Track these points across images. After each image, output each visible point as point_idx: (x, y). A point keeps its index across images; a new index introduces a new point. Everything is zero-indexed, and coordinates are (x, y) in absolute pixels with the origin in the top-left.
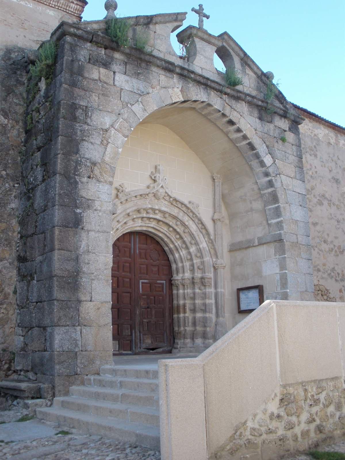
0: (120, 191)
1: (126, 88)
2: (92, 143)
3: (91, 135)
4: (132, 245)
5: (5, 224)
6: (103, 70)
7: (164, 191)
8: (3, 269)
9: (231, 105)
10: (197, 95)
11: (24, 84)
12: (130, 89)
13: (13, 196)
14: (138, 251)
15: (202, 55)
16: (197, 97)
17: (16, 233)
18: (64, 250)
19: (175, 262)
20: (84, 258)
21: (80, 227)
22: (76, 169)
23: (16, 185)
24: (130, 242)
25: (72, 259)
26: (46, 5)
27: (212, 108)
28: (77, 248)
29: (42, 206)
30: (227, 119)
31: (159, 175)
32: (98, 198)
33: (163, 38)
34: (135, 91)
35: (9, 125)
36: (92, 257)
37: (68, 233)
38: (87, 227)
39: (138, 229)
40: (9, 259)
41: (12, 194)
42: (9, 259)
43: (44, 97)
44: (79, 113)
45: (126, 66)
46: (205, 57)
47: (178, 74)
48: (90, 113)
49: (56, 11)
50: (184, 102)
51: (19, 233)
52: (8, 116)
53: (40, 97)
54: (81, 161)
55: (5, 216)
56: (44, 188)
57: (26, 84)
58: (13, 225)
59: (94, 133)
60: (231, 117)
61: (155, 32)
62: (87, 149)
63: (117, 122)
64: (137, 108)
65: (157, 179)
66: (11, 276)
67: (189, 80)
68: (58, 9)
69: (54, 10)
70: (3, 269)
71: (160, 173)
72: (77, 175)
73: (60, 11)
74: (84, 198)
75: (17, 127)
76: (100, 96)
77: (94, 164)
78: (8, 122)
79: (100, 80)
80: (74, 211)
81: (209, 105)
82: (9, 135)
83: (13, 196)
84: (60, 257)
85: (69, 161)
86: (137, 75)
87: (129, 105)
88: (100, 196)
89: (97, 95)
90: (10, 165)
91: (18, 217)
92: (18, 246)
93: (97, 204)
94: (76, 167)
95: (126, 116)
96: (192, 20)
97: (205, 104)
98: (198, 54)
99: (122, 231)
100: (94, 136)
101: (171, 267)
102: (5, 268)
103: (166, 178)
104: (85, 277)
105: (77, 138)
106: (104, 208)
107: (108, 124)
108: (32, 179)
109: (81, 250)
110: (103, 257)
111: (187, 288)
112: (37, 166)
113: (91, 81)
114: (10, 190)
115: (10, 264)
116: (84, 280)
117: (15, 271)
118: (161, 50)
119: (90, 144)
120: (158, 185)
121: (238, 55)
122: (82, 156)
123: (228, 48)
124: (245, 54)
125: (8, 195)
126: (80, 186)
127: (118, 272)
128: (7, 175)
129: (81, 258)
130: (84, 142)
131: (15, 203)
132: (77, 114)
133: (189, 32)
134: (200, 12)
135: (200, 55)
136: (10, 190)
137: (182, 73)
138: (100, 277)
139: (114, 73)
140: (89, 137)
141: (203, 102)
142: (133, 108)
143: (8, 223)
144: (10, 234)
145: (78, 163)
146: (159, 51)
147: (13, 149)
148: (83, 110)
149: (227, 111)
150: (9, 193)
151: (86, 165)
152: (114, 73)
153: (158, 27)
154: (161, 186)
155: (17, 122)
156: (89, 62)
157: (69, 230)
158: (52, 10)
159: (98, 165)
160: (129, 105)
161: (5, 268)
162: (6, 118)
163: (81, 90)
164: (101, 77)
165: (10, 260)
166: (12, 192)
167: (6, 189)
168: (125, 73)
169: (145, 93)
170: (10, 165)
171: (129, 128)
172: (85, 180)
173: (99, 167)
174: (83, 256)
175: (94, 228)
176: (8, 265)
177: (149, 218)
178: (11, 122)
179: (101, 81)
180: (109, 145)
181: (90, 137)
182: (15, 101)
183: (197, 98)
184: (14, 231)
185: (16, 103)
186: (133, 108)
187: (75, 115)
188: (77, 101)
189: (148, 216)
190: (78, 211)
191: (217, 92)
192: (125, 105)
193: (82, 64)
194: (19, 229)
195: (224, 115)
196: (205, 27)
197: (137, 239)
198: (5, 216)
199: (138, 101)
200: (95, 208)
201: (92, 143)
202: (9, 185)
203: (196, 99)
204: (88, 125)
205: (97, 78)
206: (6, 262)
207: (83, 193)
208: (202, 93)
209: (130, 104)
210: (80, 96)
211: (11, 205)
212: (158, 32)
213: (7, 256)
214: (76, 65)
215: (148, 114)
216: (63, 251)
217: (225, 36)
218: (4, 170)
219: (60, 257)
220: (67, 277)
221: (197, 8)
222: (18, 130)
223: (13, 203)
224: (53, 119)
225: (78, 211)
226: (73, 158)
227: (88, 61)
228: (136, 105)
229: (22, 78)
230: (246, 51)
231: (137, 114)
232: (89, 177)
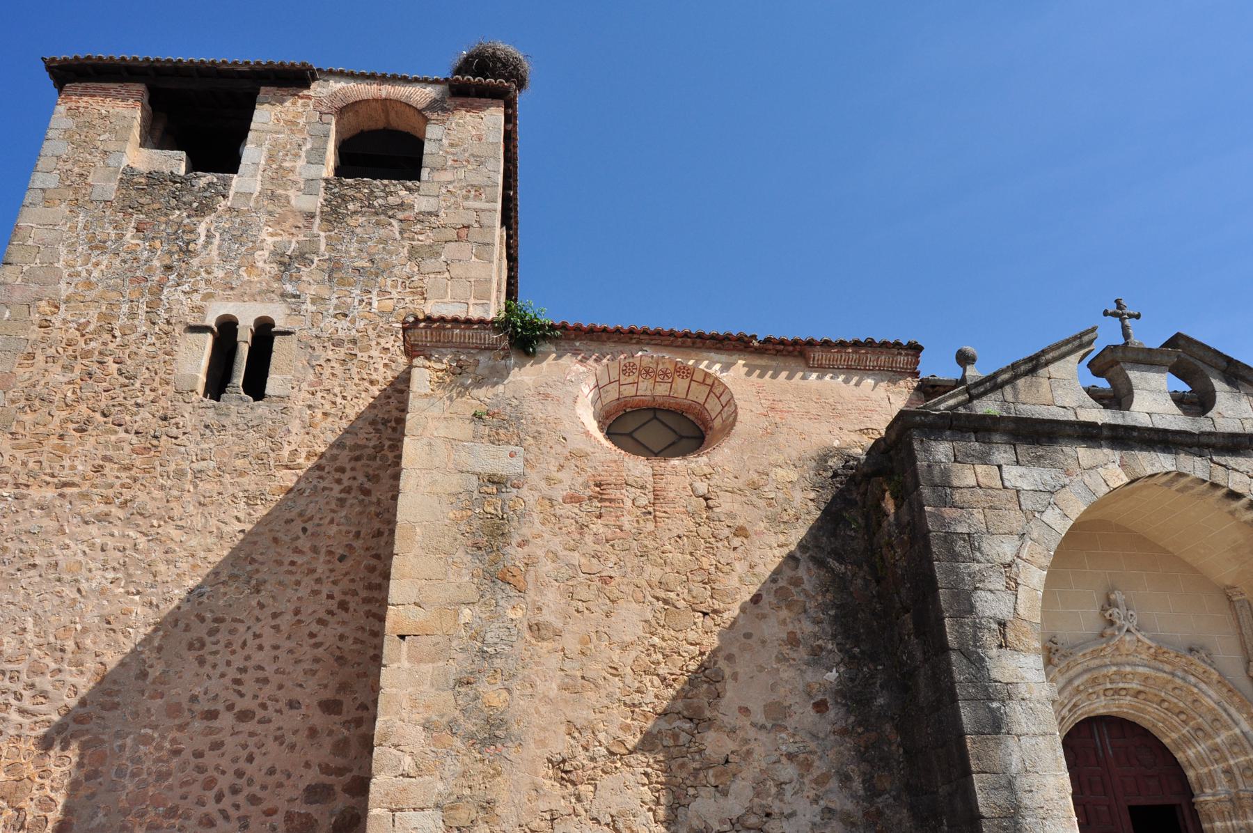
0: (1053, 650)
1: (1025, 488)
2: (991, 591)
3: (987, 577)
4: (1098, 740)
5: (874, 733)
6: (980, 469)
7: (1135, 638)
8: (886, 809)
9: (1224, 463)
10: (1153, 465)
11: (857, 503)
12: (1032, 488)
13: (878, 685)
14: (1111, 752)
15: (1143, 389)
16: (1154, 468)
17: (895, 745)
18: (986, 773)
19: (1191, 765)
20: (1022, 783)
21: (1003, 731)
22: (976, 639)
23: (880, 667)
24: (1092, 737)
25: (1001, 787)
26: (860, 369)
27: (1189, 479)
28: (1006, 767)
29: (933, 702)
30: (1224, 491)
31: (1117, 610)
32: (1023, 679)
33: (1066, 382)
34: (1042, 488)
35: (849, 573)
36: (1033, 779)
37: (987, 744)
38: (1016, 729)
39: (1102, 711)
40: (891, 790)
41: (876, 683)
42: (891, 790)
43: (896, 525)
44: (959, 546)
45: (1015, 451)
46: (1151, 391)
47: (1107, 438)
48: (976, 544)
49: (877, 374)
50: (1132, 482)
51: (899, 746)
52: (843, 559)
53: (889, 525)
54: (981, 624)
55: (873, 720)
56: (930, 672)
57: (860, 504)
58: (887, 733)
59: (991, 573)
60: (1232, 486)
61: (1049, 378)
62: (986, 602)
63: (1024, 548)
64: (1051, 516)
65: (1115, 618)
66: (900, 820)
67: (1130, 443)
68: (879, 369)
69: (874, 374)
70: (886, 809)
71: (1118, 607)
72: (979, 647)
73: (883, 372)
74: (1000, 682)
75: (861, 574)
76: (986, 511)
77: (1002, 624)
78: (846, 568)
79: (979, 485)
80: (988, 707)
81: (1180, 475)
82: (851, 589)
83: (878, 685)
84: (982, 785)
85: (961, 626)
86: (1037, 460)
87: (1037, 515)
88: (1024, 674)
89: (981, 510)
90: (864, 637)
91: (893, 719)
92: (903, 768)
93: (1023, 690)
94: (975, 635)
95: (1035, 535)
96: (1109, 334)
97: (1172, 475)
98: (1135, 391)
99: (1072, 718)
100: (992, 579)
101: (1186, 776)
102: (887, 806)
103: (1132, 613)
104: (1031, 816)
105: (966, 588)
106: (1036, 695)
107: (1009, 554)
108: (904, 658)
109: (1014, 769)
110: (1052, 778)
111: (1230, 816)
112: (909, 636)
113: (965, 490)
114: (872, 676)
115: (895, 800)
116: (1029, 820)
117: (905, 811)
118: (1066, 405)
119: (989, 593)
120: (1120, 629)
121: (1215, 367)
122: (980, 615)
123: (1192, 360)
124: (1229, 360)
125: (870, 685)
126: (989, 664)
127: (1082, 794)
128: (862, 652)
129: (1018, 783)
130: (979, 592)
131: (883, 697)
132: (957, 549)
133: (1109, 357)
134: (1118, 312)
135: (1139, 392)
136: (872, 676)
137: (1114, 434)
138: (1055, 812)
139: (1000, 467)
140: (984, 581)
141: (1167, 473)
142: (1044, 518)
143: (879, 731)
144: (886, 749)
145: (977, 627)
146: (1065, 407)
147: (863, 610)
148: (964, 540)
149: (1219, 476)
150: (871, 682)
151: (989, 629)
152: (1000, 467)
153: (1052, 368)
154: (1125, 630)
155: (860, 567)
156: (956, 461)
157: (988, 739)
158: (872, 375)
159: (1009, 624)
160: (1037, 515)
161: (887, 806)
162: (841, 564)
163: (954, 509)
164: (981, 480)
165: (894, 793)
166: (875, 680)
167: (865, 676)
168: (1018, 463)
169: (1057, 488)
170: (864, 637)
171: (1046, 552)
172: (994, 652)
173: (1013, 627)
174: (1019, 779)
175: (1025, 730)
176: (891, 800)
177: (1117, 692)
178: (850, 567)
179: (981, 487)
180: (1020, 589)
181: (986, 581)
182: (848, 533)
183: (1155, 470)
184: (890, 744)
185: (851, 536)
186: (1044, 518)
187: (954, 551)
188: (952, 528)
189: (1114, 686)
190: (995, 705)
191: (1190, 447)
192: (1030, 515)
193: (945, 468)
194: (899, 739)
195: (1215, 486)
196: (1135, 340)
197: (1105, 729)
198: (873, 720)
199: (1049, 504)
200: (1020, 696)
201: (991, 591)
202: (869, 668)
203: (1152, 473)
204: (978, 562)
205: (974, 483)
206: (887, 796)
207: (995, 674)
208: (1161, 458)
209: (1039, 512)
210: (954, 519)
211: (878, 700)
212: (1054, 374)
213: (888, 787)
214: (936, 471)
215: (1072, 522)
216: (984, 775)
217: (1177, 341)
218: (855, 646)
219: (982, 785)
220: (999, 817)
221: (1112, 308)
222: (864, 578)
223: (880, 697)
224: (920, 561)
225: (995, 705)
226: (966, 620)
227: (953, 459)
228: (1049, 511)
229: (852, 494)
230: (1228, 355)
231: (1053, 526)
232: (1000, 646)
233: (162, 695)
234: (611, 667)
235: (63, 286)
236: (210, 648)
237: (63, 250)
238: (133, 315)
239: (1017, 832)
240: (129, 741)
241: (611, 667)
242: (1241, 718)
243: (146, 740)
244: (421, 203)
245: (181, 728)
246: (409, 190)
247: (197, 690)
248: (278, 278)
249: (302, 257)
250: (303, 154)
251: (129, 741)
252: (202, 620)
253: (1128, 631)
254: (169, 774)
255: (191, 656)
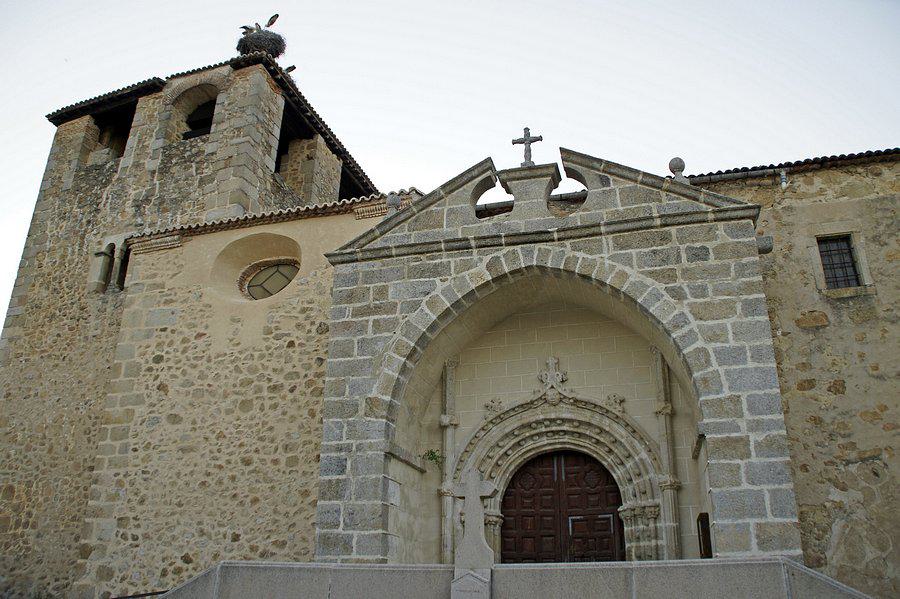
4: (556, 468)
233: (73, 459)
234: (704, 519)
235: (48, 243)
236: (93, 433)
237: (49, 223)
238: (73, 252)
239: (899, 305)
240: (60, 483)
241: (704, 519)
242: (747, 520)
243: (66, 482)
244: (209, 148)
245: (79, 475)
246: (204, 141)
247: (87, 456)
248: (134, 216)
249: (147, 200)
250: (154, 134)
251: (60, 483)
252: (90, 418)
253: (552, 387)
254: (73, 500)
255: (85, 438)
